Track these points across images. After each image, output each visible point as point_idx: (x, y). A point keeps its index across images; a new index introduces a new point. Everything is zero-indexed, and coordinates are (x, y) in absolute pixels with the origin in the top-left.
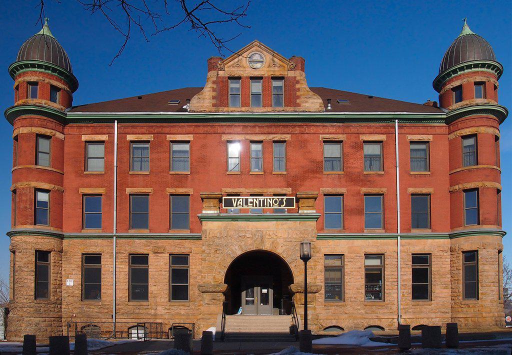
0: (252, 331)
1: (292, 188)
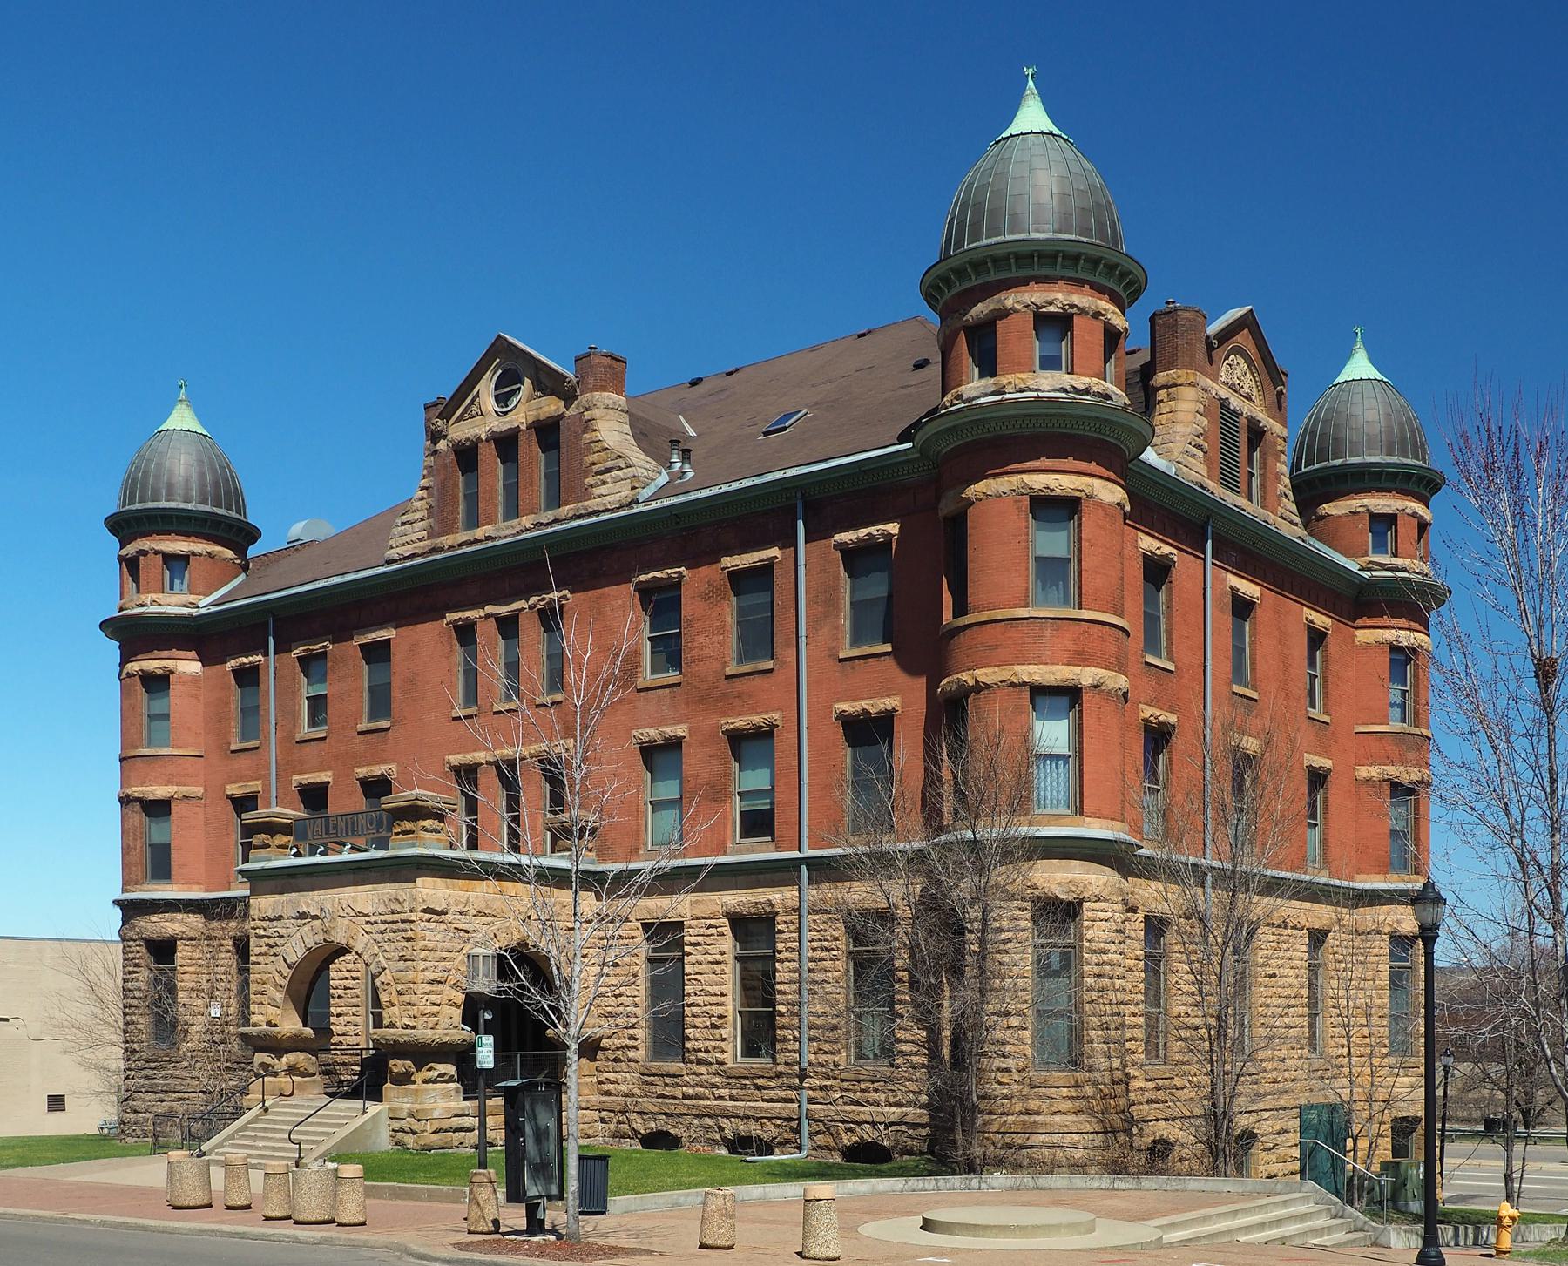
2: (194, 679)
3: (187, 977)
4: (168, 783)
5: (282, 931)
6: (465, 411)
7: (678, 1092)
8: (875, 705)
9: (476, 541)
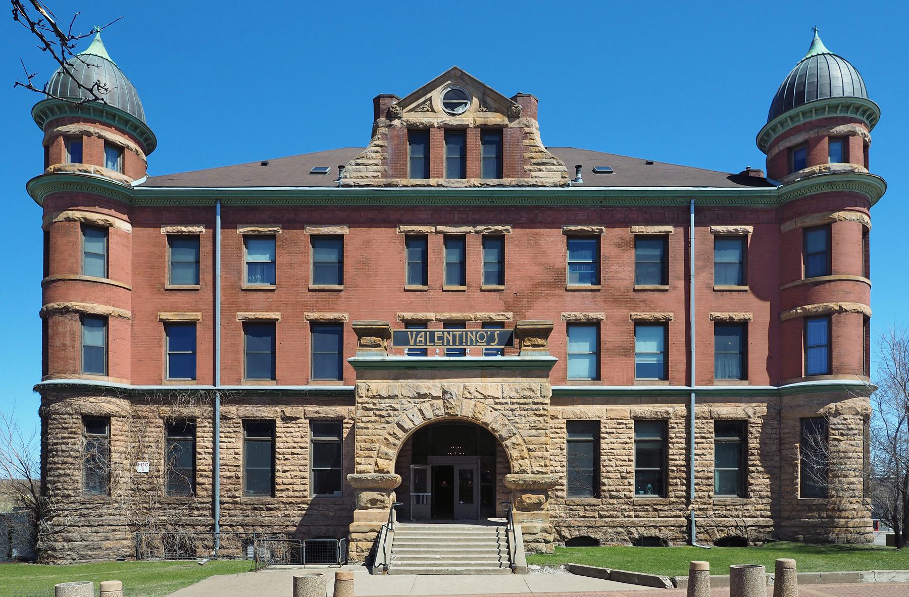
0: (498, 591)
1: (514, 312)
2: (126, 235)
3: (118, 443)
4: (107, 303)
5: (396, 406)
6: (418, 106)
7: (596, 514)
8: (738, 316)
9: (429, 186)
